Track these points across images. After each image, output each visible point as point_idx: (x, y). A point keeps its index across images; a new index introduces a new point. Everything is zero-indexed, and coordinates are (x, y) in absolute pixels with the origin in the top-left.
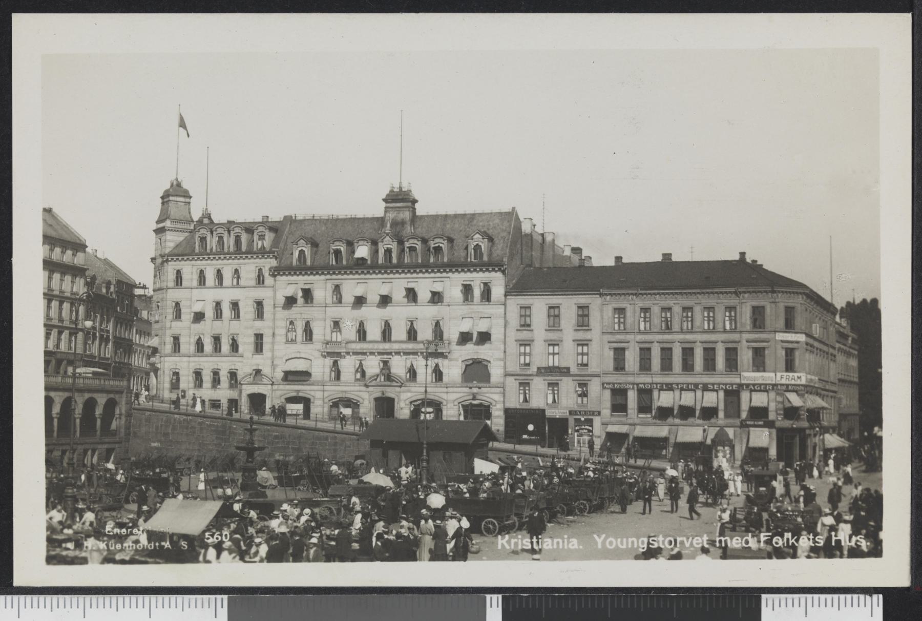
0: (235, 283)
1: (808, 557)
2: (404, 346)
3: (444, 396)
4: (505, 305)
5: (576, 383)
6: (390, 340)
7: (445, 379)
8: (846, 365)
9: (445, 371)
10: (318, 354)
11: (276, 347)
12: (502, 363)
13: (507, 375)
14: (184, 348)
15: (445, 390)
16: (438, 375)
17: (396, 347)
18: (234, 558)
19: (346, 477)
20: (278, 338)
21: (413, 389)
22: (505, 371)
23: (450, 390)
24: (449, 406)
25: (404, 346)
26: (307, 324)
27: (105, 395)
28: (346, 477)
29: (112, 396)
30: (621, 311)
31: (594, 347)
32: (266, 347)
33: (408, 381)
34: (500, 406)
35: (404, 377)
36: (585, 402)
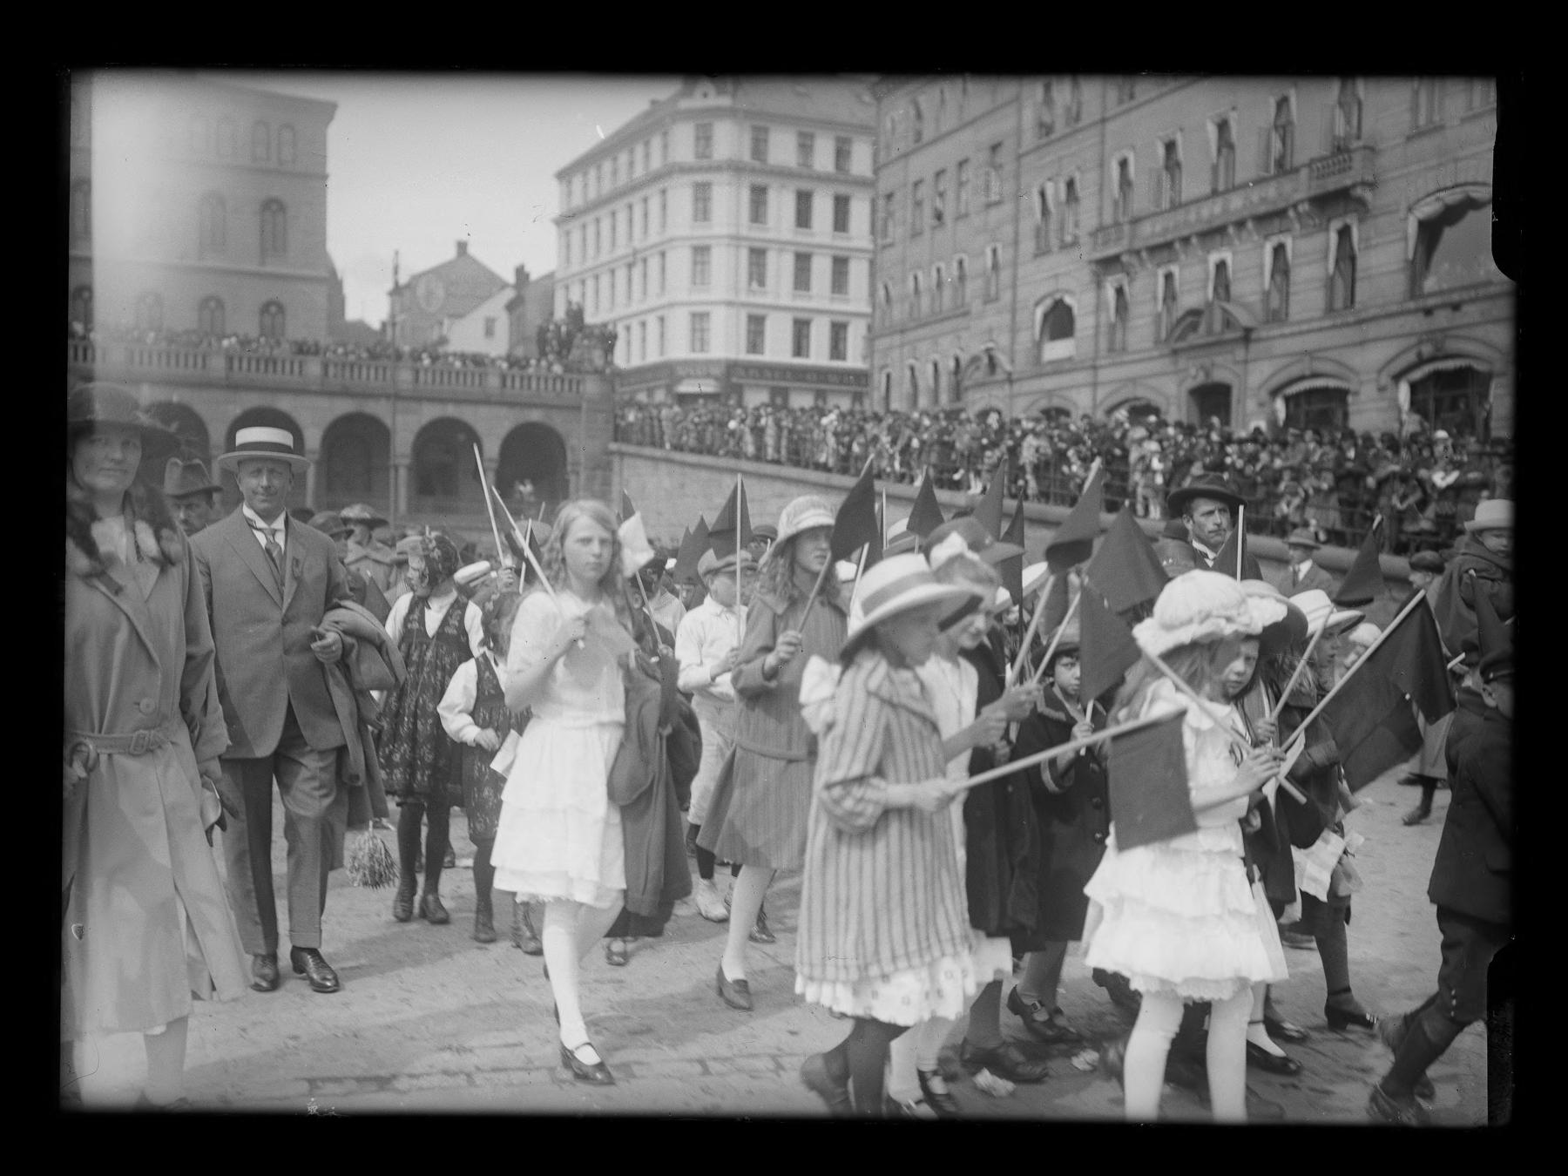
21: (1280, 346)
27: (503, 411)
29: (535, 416)
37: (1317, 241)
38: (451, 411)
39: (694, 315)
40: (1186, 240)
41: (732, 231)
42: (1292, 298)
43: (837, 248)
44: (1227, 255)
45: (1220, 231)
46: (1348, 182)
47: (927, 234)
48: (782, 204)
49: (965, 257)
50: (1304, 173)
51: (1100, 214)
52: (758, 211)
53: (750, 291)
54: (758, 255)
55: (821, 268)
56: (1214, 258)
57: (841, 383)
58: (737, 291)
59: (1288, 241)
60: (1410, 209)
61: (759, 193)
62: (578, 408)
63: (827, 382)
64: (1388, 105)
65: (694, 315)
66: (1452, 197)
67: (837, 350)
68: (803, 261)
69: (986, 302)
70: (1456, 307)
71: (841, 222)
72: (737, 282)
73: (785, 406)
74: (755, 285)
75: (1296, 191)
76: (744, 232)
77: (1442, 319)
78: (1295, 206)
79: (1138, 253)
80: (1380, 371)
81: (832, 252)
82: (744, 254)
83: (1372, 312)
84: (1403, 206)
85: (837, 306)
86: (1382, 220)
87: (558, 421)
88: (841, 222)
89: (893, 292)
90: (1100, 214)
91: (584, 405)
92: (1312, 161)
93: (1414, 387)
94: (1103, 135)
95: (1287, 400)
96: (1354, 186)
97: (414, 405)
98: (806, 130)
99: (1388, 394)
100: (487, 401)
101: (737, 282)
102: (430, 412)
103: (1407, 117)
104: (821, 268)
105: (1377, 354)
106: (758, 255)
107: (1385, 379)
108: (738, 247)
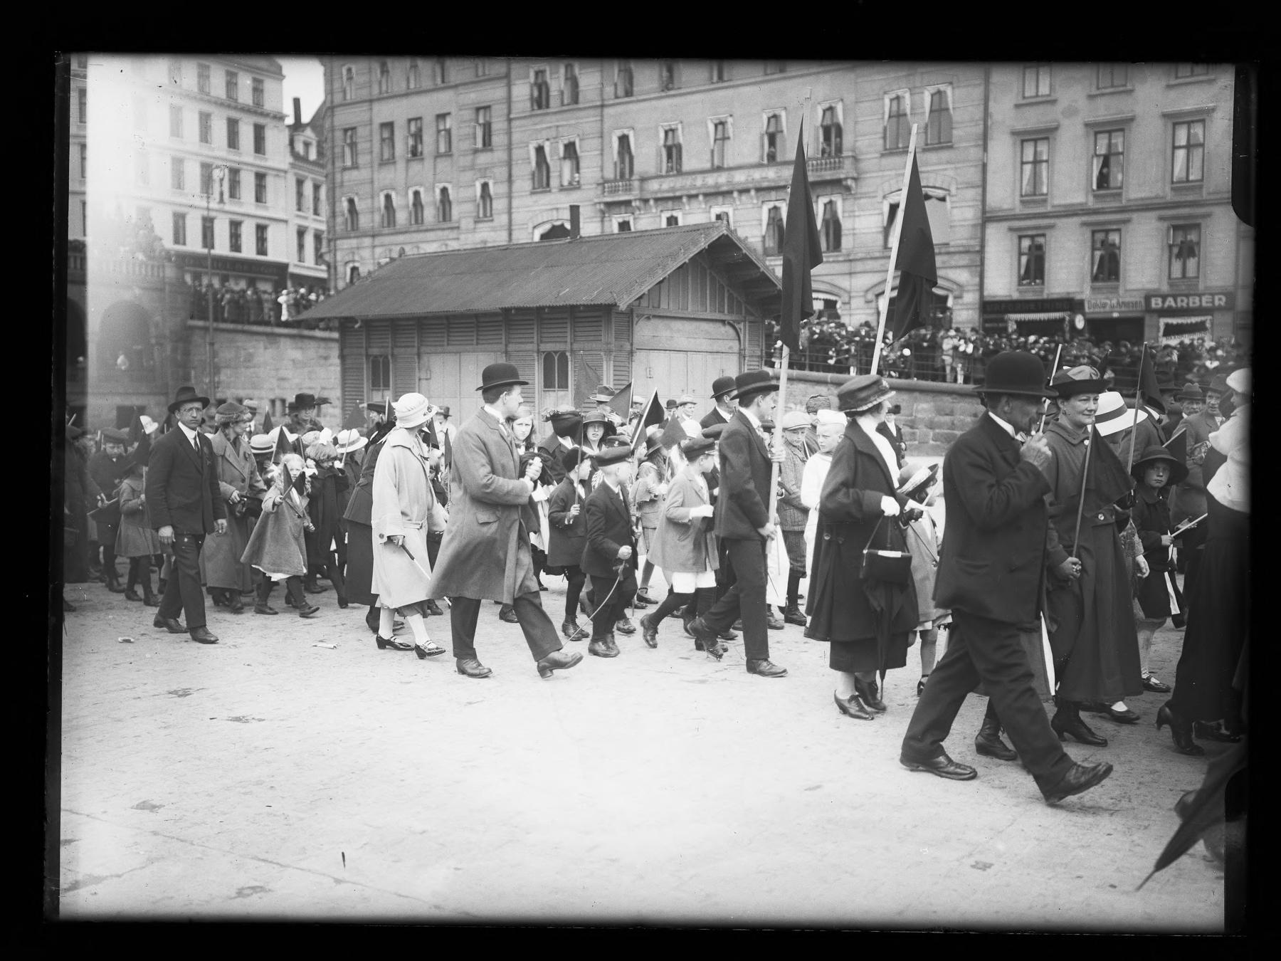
2: (757, 174)
3: (844, 282)
5: (1166, 224)
7: (846, 242)
8: (244, 291)
9: (846, 224)
11: (515, 203)
12: (973, 194)
13: (987, 217)
14: (364, 221)
15: (845, 267)
17: (740, 178)
18: (1218, 878)
19: (232, 512)
20: (517, 185)
22: (984, 211)
23: (859, 266)
25: (757, 174)
26: (624, 140)
28: (232, 512)
32: (499, 205)
34: (971, 297)
36: (1191, 272)
40: (691, 197)
43: (258, 166)
45: (727, 194)
46: (842, 176)
47: (401, 165)
49: (422, 190)
55: (247, 181)
60: (884, 197)
64: (1152, 94)
69: (476, 222)
71: (259, 147)
73: (329, 266)
75: (352, 251)
79: (646, 201)
80: (867, 291)
81: (255, 169)
83: (860, 255)
84: (880, 194)
86: (862, 201)
88: (259, 147)
89: (359, 205)
94: (602, 116)
96: (846, 179)
103: (881, 142)
104: (247, 181)
105: (863, 282)
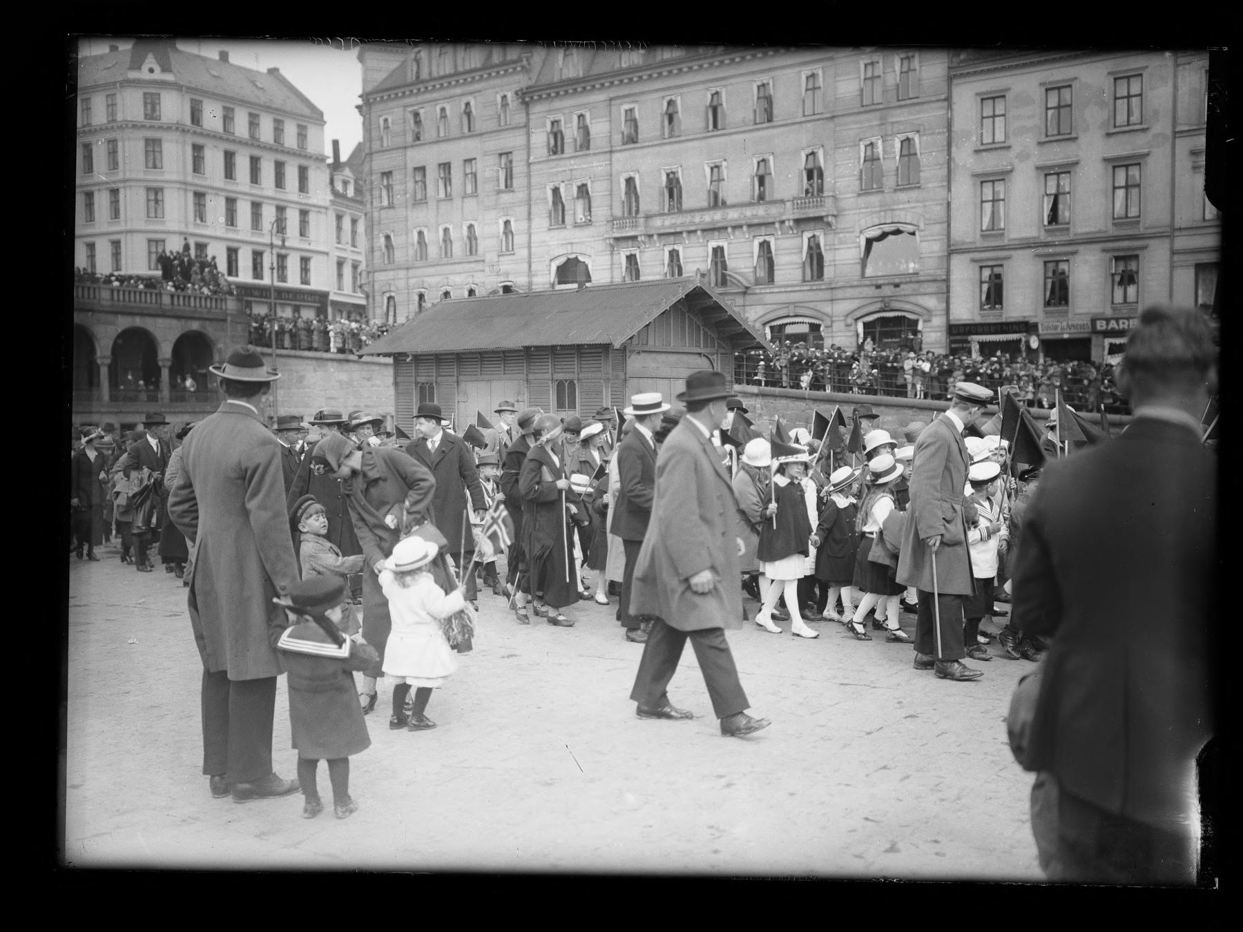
0: (466, 130)
1: (384, 417)
3: (827, 308)
4: (948, 100)
5: (1109, 255)
6: (1057, 223)
7: (828, 272)
10: (600, 246)
13: (952, 250)
15: (827, 295)
16: (816, 260)
17: (733, 215)
21: (769, 298)
23: (839, 294)
24: (836, 326)
27: (174, 322)
29: (195, 326)
30: (813, 76)
31: (1156, 171)
33: (758, 282)
34: (939, 321)
35: (751, 277)
37: (794, 242)
38: (138, 322)
39: (150, 241)
41: (181, 178)
42: (776, 273)
44: (723, 243)
46: (823, 214)
48: (214, 159)
50: (789, 205)
51: (611, 207)
52: (198, 165)
53: (195, 225)
54: (199, 196)
55: (244, 211)
56: (713, 244)
57: (261, 296)
58: (186, 225)
59: (772, 240)
61: (197, 149)
62: (224, 320)
63: (252, 295)
65: (150, 241)
66: (887, 228)
67: (257, 270)
68: (231, 202)
70: (897, 286)
72: (186, 217)
74: (198, 221)
76: (190, 179)
77: (887, 291)
78: (782, 222)
79: (651, 236)
82: (191, 196)
85: (230, 235)
87: (211, 330)
90: (611, 207)
91: (229, 319)
92: (794, 198)
93: (865, 324)
95: (771, 328)
97: (111, 317)
98: (254, 112)
99: (852, 328)
100: (164, 315)
101: (186, 217)
102: (124, 323)
104: (244, 211)
105: (843, 307)
106: (199, 196)
107: (850, 320)
108: (186, 190)
